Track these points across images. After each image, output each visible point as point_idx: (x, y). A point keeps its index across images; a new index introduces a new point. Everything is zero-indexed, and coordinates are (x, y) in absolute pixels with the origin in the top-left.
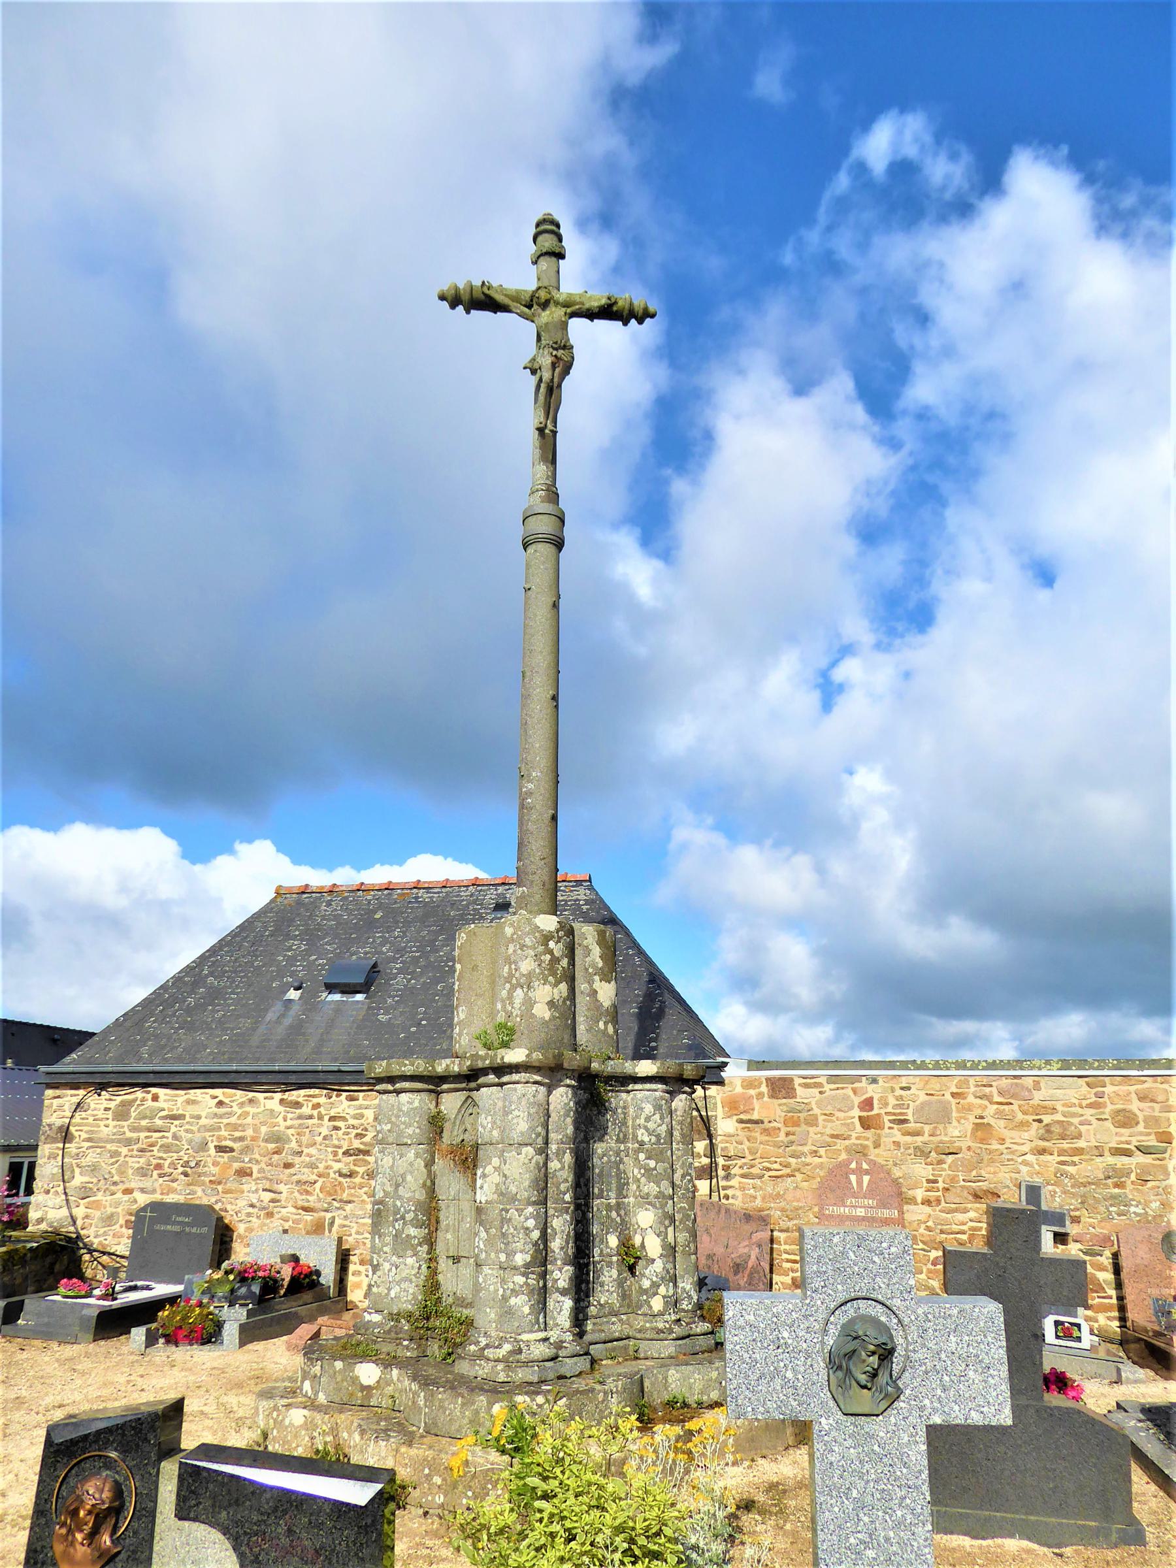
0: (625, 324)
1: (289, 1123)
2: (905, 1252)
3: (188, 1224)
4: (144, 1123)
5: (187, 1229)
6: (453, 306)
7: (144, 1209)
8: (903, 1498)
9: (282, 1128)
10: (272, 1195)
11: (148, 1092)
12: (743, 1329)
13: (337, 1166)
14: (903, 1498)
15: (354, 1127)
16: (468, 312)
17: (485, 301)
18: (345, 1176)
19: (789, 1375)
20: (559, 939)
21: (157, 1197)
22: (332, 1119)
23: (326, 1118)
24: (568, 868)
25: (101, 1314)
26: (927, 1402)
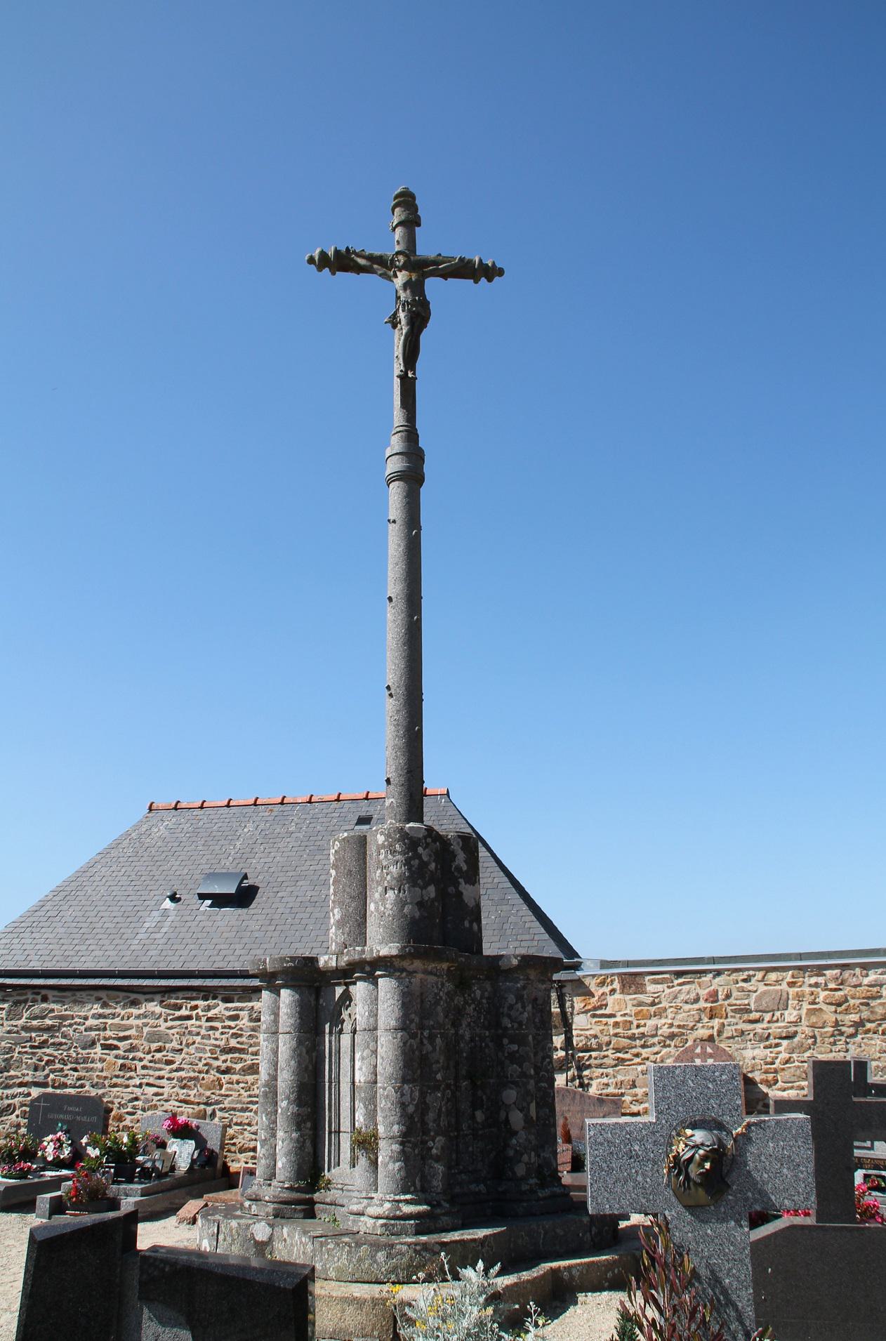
0: (476, 282)
1: (170, 1024)
2: (733, 1078)
3: (78, 1113)
4: (35, 1023)
5: (78, 1118)
6: (320, 268)
7: (38, 1099)
8: (730, 1270)
9: (162, 1028)
10: (155, 1090)
11: (38, 994)
12: (602, 1144)
13: (216, 1063)
14: (730, 1270)
15: (230, 1027)
16: (334, 274)
17: (342, 262)
18: (224, 1072)
19: (640, 1178)
20: (427, 845)
21: (135, 1011)
22: (209, 1019)
23: (204, 1019)
24: (433, 782)
25: (6, 1188)
26: (750, 1194)
